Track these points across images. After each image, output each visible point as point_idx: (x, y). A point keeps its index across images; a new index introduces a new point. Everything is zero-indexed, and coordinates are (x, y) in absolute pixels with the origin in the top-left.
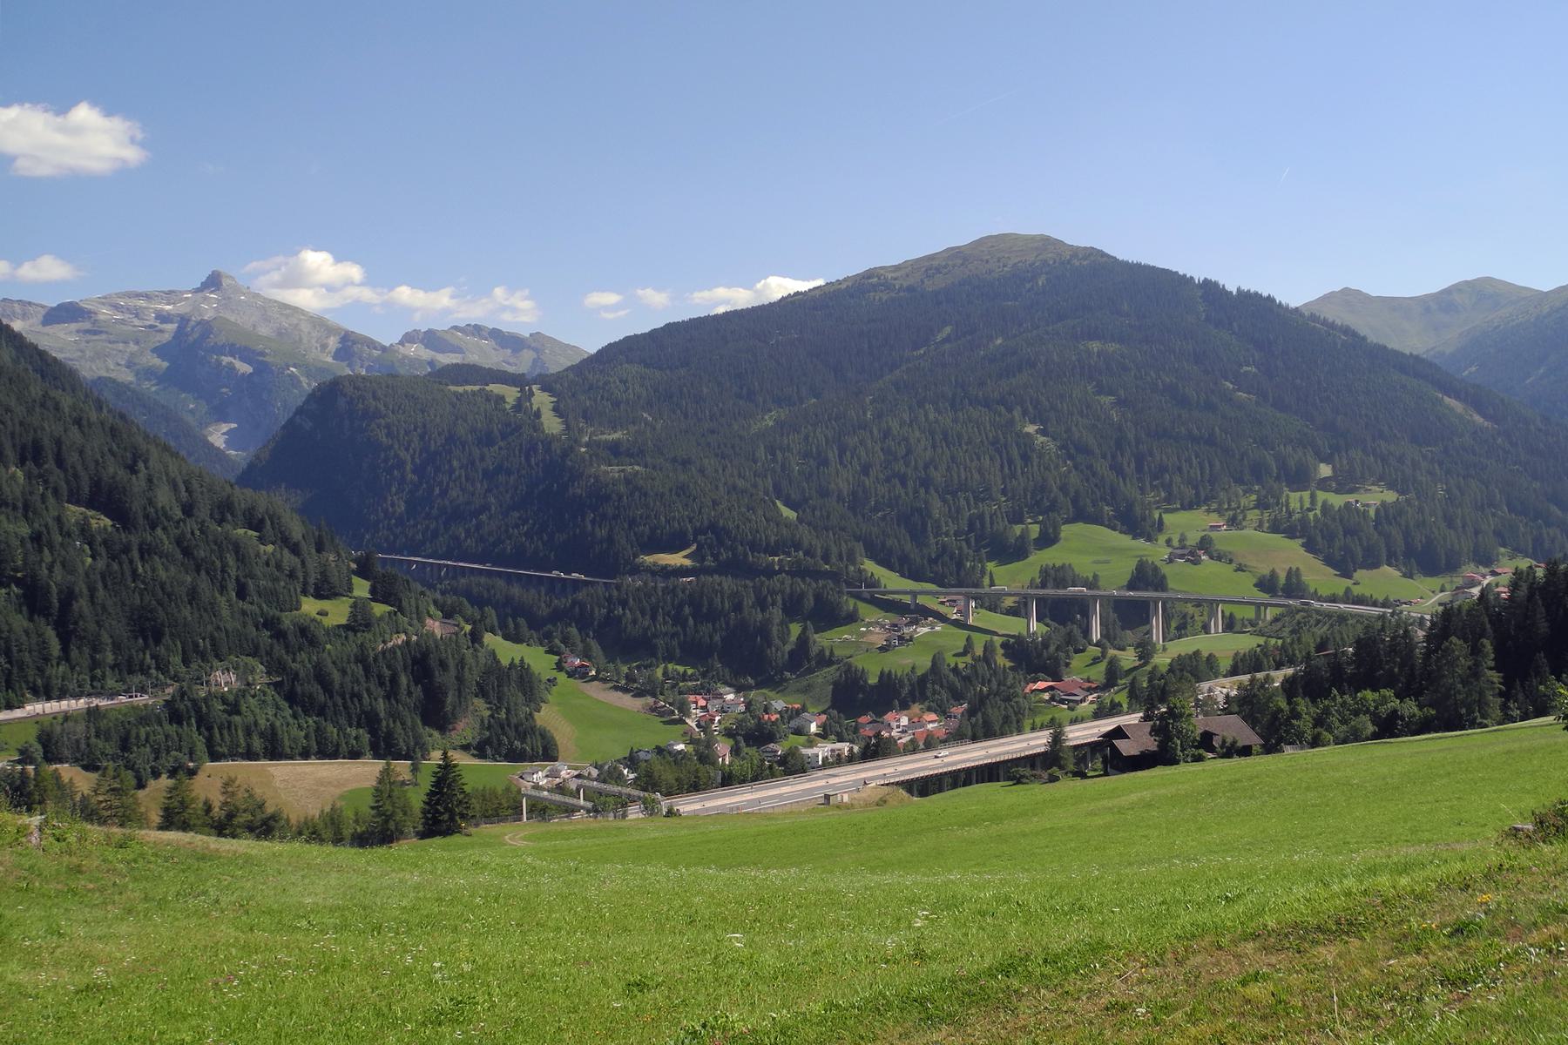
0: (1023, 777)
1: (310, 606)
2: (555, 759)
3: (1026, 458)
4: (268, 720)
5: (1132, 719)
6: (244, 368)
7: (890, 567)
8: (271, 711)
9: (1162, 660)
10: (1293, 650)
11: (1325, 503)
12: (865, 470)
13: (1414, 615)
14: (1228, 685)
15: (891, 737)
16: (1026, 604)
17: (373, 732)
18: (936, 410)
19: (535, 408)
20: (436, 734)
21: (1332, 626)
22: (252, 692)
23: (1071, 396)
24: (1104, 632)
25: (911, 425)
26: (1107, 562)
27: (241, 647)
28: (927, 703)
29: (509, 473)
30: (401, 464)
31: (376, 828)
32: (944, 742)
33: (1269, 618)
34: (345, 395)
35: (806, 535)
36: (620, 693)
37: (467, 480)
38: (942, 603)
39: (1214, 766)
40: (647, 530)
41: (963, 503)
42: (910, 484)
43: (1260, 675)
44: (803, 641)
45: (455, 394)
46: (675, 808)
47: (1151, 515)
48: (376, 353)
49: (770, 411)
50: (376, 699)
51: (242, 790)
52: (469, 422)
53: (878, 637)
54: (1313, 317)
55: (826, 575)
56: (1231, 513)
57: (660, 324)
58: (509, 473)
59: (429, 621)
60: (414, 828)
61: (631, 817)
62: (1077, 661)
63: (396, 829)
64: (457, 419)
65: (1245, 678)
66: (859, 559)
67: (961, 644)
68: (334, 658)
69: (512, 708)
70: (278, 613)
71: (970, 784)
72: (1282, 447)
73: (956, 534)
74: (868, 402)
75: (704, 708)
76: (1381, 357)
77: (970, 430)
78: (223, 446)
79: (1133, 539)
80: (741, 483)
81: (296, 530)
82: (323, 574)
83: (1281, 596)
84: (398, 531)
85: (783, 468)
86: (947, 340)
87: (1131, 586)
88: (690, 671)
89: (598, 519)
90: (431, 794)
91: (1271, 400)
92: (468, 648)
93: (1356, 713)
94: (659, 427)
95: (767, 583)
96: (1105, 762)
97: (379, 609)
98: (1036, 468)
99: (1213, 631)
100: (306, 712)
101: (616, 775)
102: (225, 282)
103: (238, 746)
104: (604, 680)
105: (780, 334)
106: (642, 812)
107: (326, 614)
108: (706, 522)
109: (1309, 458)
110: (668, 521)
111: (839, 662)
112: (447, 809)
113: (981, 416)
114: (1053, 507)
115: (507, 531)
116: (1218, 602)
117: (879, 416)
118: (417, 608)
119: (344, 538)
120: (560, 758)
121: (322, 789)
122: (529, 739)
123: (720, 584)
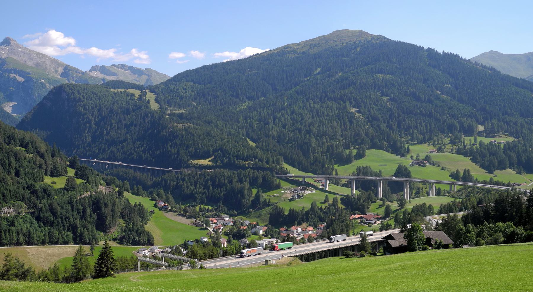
0: (349, 254)
1: (48, 180)
2: (152, 244)
3: (351, 122)
4: (27, 228)
5: (395, 231)
6: (20, 79)
7: (294, 166)
8: (28, 225)
9: (409, 207)
10: (467, 204)
11: (480, 142)
12: (284, 127)
13: (522, 190)
14: (438, 218)
15: (294, 237)
16: (351, 182)
17: (74, 233)
18: (314, 102)
19: (147, 99)
20: (102, 234)
21: (484, 194)
22: (21, 216)
23: (370, 97)
24: (384, 195)
25: (303, 108)
26: (386, 165)
27: (16, 197)
28: (309, 223)
29: (136, 125)
30: (89, 121)
31: (74, 274)
32: (316, 239)
33: (456, 190)
34: (66, 92)
35: (259, 152)
36: (181, 217)
37: (118, 128)
38: (316, 181)
39: (431, 252)
40: (194, 150)
41: (324, 140)
42: (303, 132)
43: (452, 214)
44: (258, 196)
45: (113, 92)
46: (203, 265)
47: (404, 146)
48: (79, 75)
49: (245, 102)
50: (76, 219)
51: (14, 259)
52: (119, 104)
53: (289, 195)
54: (477, 63)
55: (267, 169)
56: (439, 146)
57: (200, 66)
58: (136, 125)
59: (100, 187)
60: (91, 274)
61: (184, 269)
62: (373, 206)
63: (83, 275)
64: (114, 103)
65: (445, 215)
66: (281, 163)
67: (324, 198)
68: (58, 202)
69: (135, 223)
70: (33, 183)
71: (327, 257)
72: (462, 118)
73: (322, 153)
74: (286, 99)
75: (216, 224)
76: (507, 80)
77: (328, 111)
78: (10, 112)
79: (396, 156)
80: (232, 131)
81: (43, 148)
82: (55, 166)
83: (461, 181)
84: (88, 149)
85: (250, 125)
86: (319, 73)
87: (395, 175)
88: (210, 208)
89: (173, 145)
90: (99, 259)
91: (457, 99)
92: (117, 198)
93: (496, 232)
94: (199, 108)
95: (243, 172)
96: (384, 249)
97: (79, 181)
98: (355, 126)
99: (431, 195)
100: (45, 225)
101: (178, 251)
102: (12, 42)
103: (13, 240)
104: (174, 212)
105: (250, 71)
106: (189, 267)
107: (55, 183)
108: (218, 148)
109: (474, 123)
110: (202, 146)
111: (272, 205)
112: (105, 266)
113: (332, 105)
114: (362, 142)
115: (135, 149)
116: (433, 183)
117: (290, 105)
118: (95, 181)
119: (64, 151)
120: (155, 244)
121: (50, 258)
122: (142, 237)
123: (223, 172)
